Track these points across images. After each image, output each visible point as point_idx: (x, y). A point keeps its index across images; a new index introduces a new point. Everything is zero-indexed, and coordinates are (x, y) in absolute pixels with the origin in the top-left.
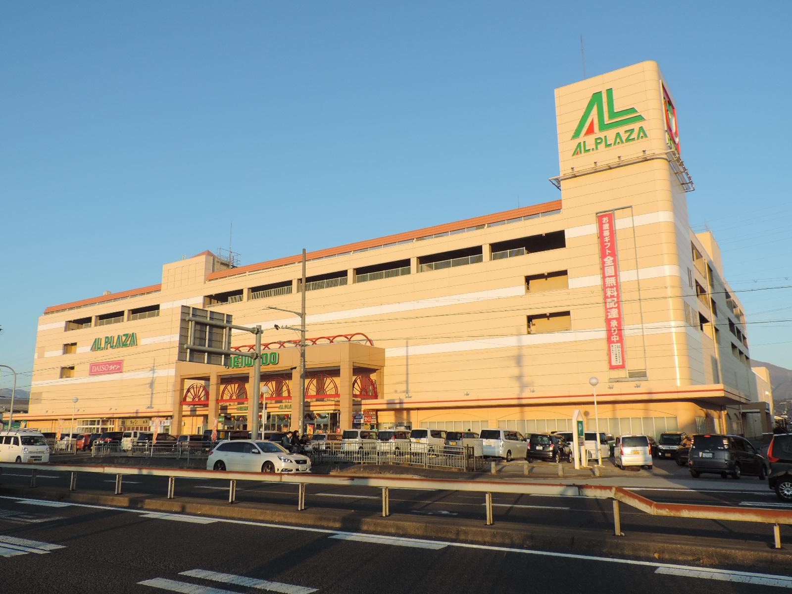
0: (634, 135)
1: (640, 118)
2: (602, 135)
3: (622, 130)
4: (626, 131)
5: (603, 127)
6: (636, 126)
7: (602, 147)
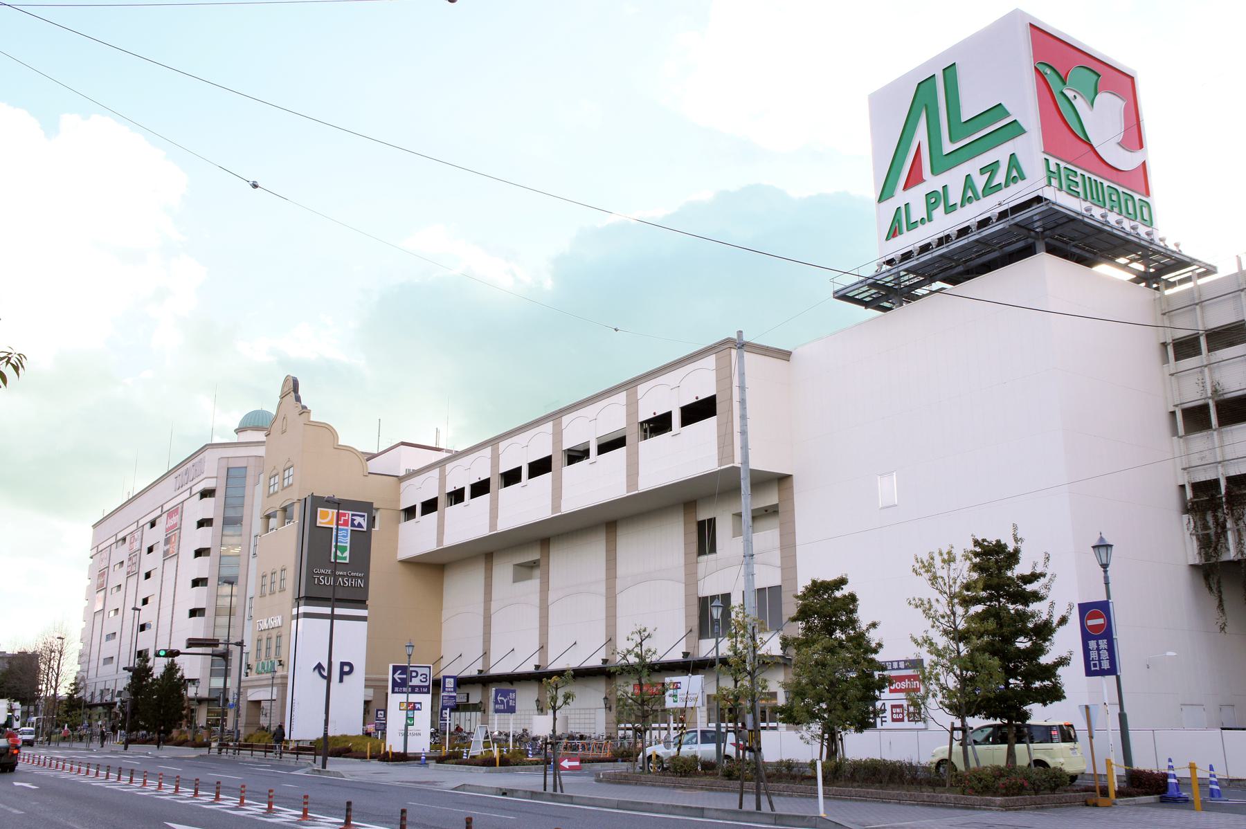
0: (1000, 178)
1: (1015, 130)
2: (932, 183)
3: (972, 167)
4: (982, 171)
5: (942, 163)
6: (1000, 155)
7: (939, 212)
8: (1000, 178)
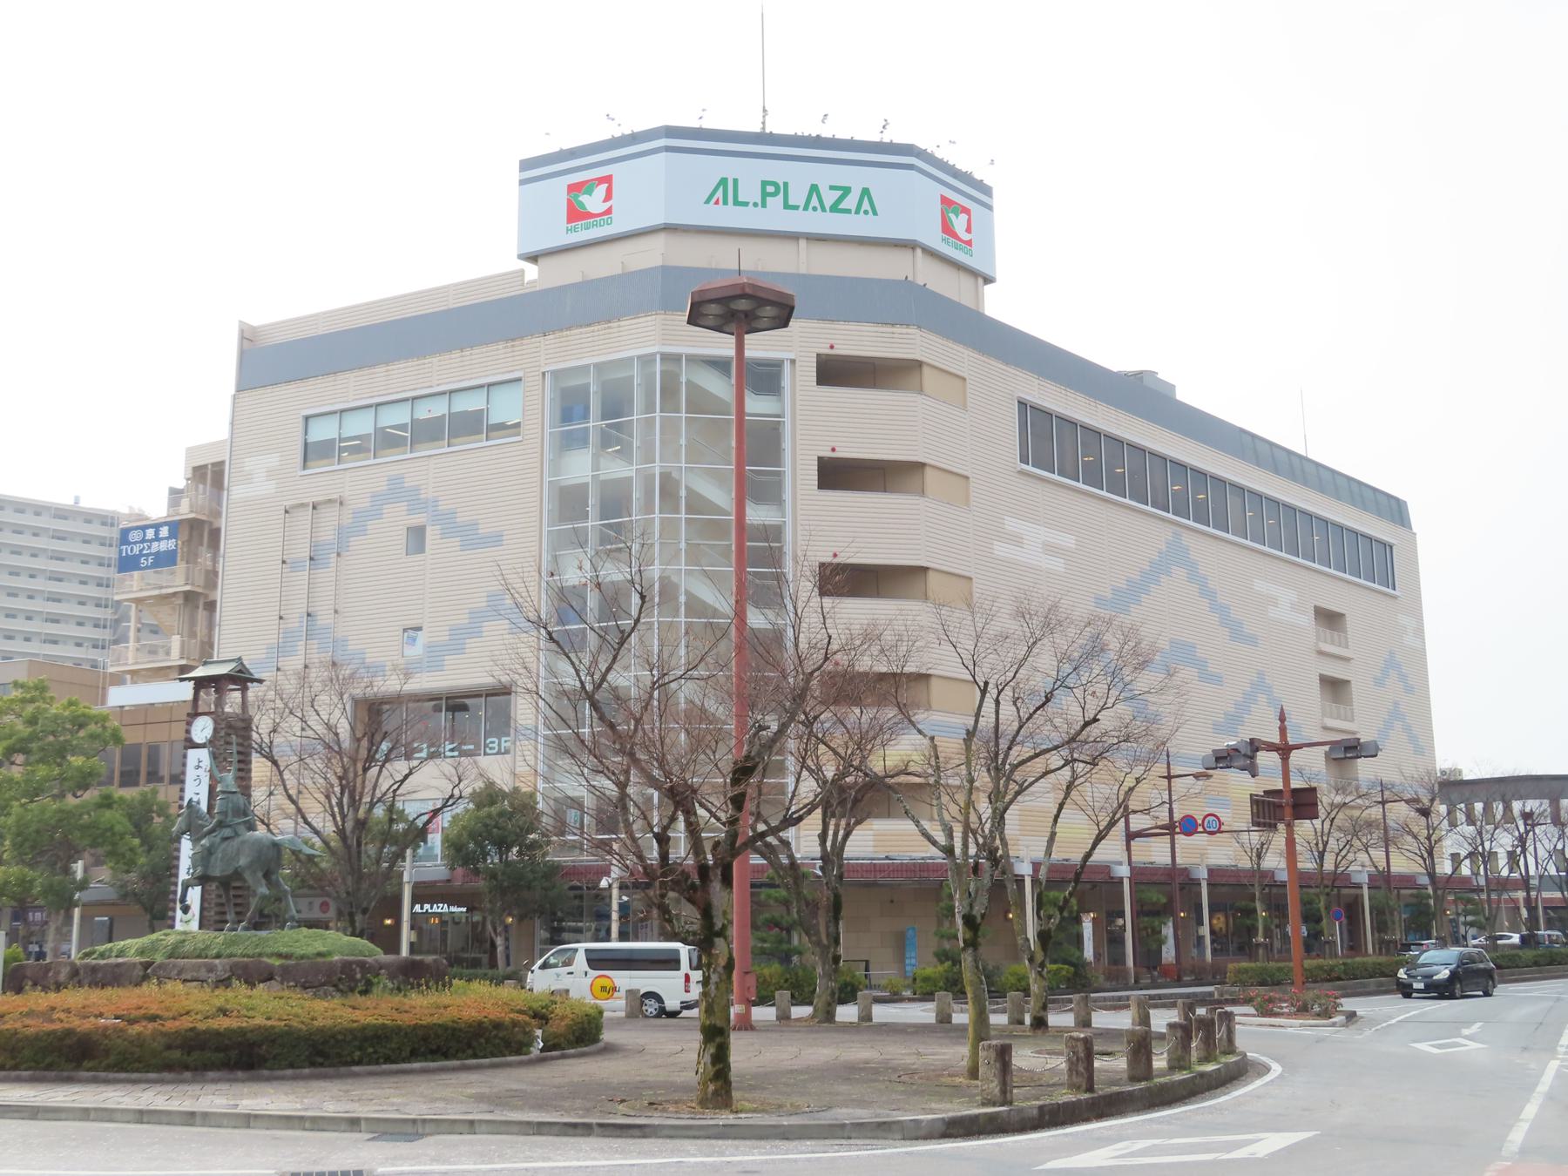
7: (775, 202)
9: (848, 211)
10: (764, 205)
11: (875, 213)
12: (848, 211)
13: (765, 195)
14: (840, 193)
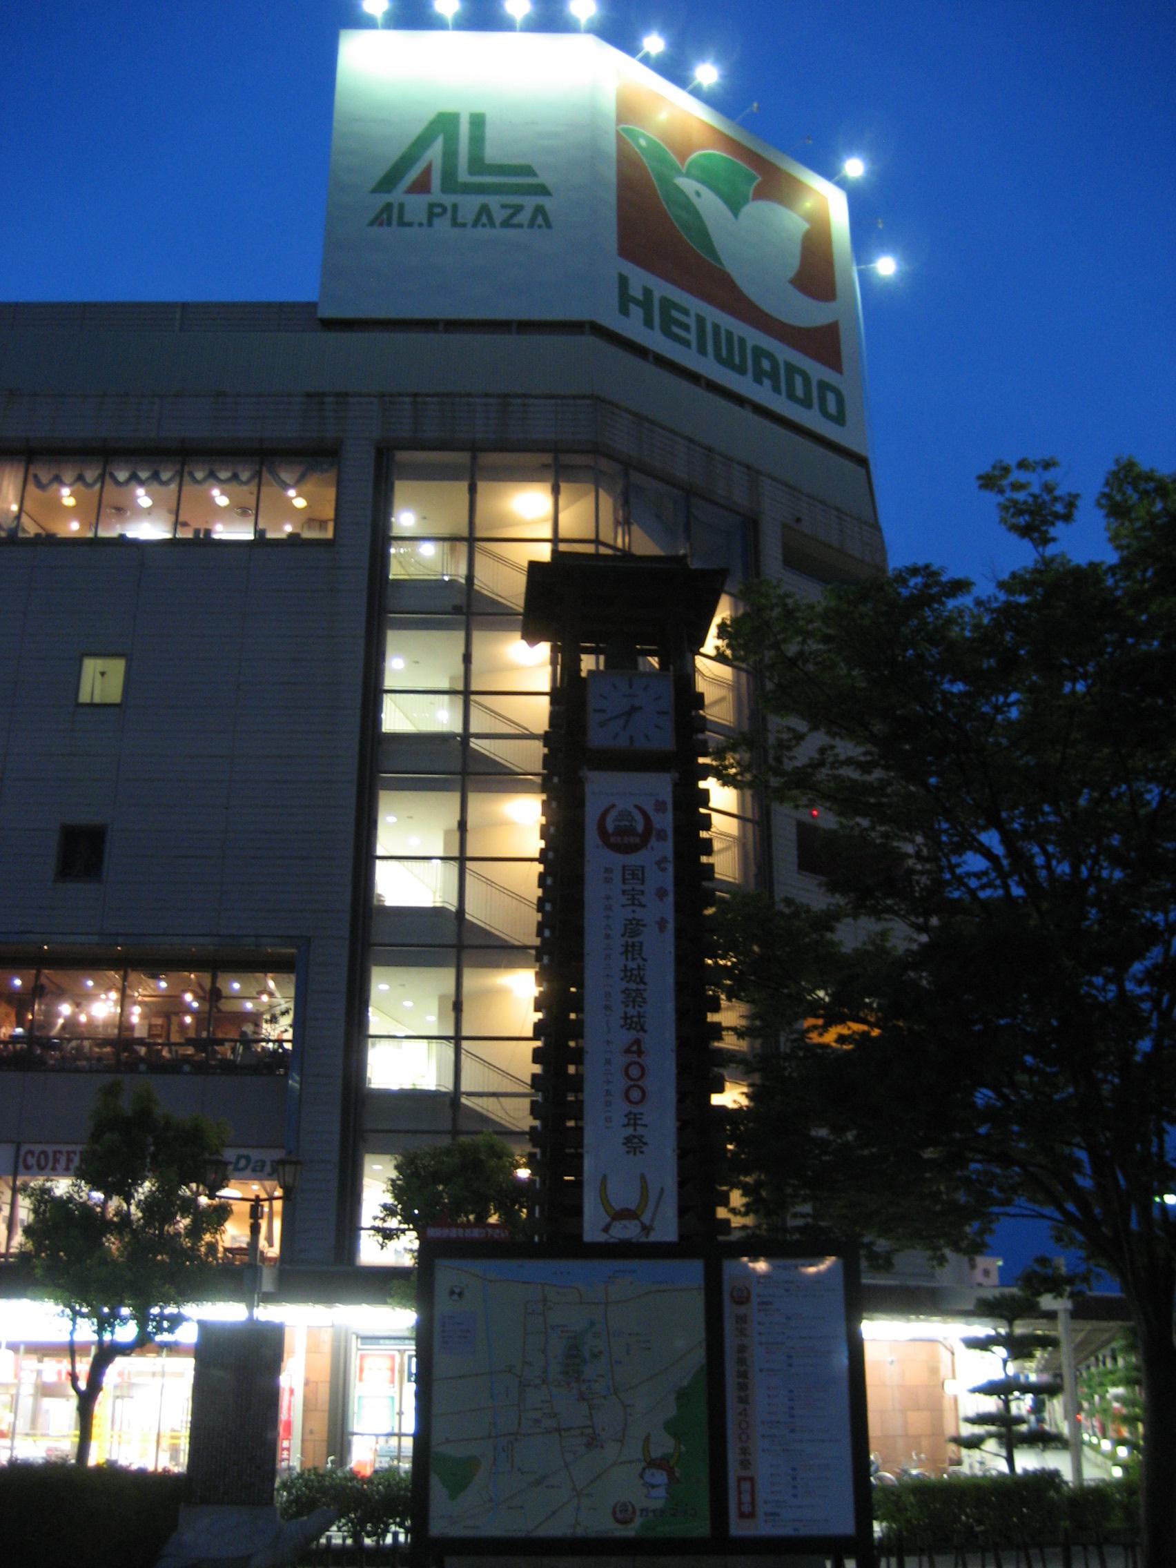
0: (524, 217)
3: (494, 202)
6: (530, 202)
7: (443, 224)
8: (524, 217)
9: (520, 226)
10: (430, 224)
11: (549, 226)
12: (520, 226)
13: (431, 215)
14: (510, 211)
